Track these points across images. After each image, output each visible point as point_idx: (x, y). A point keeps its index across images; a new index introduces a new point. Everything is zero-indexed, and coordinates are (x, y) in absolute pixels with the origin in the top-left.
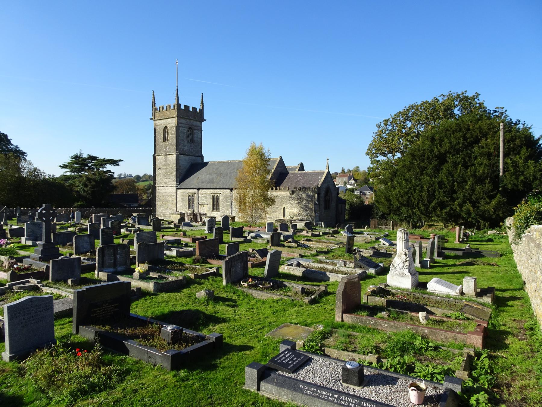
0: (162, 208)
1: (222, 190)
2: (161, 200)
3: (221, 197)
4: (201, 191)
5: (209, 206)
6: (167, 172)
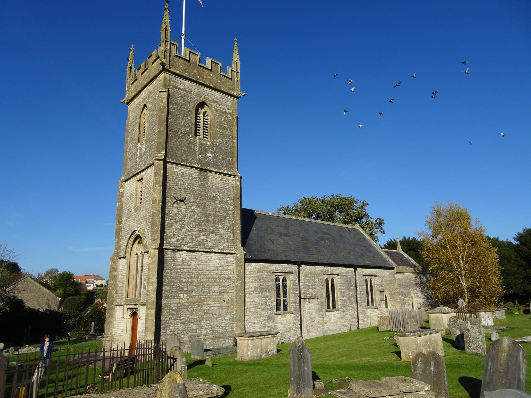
0: (185, 315)
1: (340, 268)
2: (182, 290)
3: (338, 281)
4: (303, 267)
5: (320, 300)
6: (206, 215)
